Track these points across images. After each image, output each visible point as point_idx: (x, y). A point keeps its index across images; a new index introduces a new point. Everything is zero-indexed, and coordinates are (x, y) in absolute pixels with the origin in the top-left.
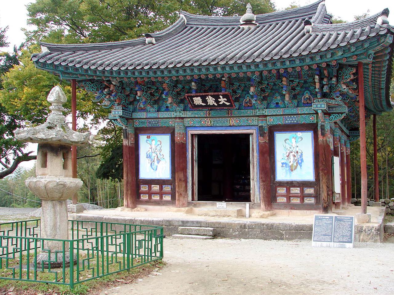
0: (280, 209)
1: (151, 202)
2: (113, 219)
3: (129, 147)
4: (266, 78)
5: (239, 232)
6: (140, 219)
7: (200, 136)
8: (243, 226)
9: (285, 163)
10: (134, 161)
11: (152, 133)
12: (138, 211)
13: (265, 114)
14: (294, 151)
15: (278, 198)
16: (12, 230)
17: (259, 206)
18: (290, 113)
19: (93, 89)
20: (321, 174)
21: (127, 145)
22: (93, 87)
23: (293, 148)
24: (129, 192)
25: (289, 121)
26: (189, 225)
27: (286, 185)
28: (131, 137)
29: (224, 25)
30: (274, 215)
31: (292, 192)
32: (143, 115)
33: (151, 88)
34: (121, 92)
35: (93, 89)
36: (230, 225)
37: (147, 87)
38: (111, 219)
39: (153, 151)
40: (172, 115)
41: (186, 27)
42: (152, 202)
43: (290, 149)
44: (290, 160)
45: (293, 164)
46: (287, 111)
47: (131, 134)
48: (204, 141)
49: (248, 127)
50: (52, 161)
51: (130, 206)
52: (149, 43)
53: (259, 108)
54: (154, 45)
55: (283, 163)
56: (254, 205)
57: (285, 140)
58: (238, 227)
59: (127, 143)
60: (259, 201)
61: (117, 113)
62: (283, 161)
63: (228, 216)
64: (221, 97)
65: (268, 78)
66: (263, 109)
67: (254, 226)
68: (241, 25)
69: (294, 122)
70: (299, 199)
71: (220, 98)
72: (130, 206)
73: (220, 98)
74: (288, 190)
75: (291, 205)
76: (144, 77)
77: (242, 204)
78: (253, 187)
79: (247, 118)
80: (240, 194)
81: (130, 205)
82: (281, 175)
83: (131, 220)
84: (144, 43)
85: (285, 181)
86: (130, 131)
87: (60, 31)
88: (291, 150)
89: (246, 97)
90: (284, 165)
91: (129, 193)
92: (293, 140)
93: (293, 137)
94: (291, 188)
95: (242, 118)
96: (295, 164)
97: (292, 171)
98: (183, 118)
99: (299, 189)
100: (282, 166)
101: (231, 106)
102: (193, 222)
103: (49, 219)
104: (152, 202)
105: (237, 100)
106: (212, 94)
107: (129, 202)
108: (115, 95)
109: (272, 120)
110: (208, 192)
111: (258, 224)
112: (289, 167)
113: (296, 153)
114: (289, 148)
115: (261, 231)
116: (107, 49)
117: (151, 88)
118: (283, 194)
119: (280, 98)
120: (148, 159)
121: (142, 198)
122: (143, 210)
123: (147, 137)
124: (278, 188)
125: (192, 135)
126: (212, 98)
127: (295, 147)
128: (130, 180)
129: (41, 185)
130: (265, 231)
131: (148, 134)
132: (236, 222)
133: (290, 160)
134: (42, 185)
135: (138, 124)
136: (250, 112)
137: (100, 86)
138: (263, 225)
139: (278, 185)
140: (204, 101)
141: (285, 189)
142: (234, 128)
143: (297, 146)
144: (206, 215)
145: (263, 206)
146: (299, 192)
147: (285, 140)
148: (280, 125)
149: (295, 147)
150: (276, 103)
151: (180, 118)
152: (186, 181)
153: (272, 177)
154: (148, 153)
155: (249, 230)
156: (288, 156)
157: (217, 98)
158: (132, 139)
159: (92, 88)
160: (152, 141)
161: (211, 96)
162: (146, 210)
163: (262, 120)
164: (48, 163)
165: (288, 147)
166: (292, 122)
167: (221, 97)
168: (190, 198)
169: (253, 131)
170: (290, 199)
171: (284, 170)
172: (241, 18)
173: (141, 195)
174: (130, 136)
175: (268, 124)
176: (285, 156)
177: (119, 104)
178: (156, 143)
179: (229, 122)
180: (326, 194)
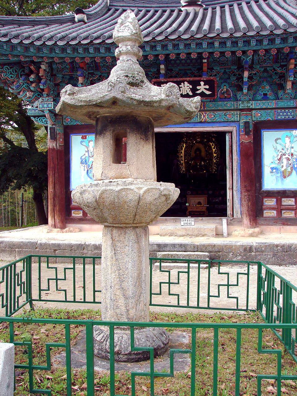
0: (268, 225)
1: (86, 220)
2: (53, 244)
3: (58, 151)
4: (259, 61)
5: (243, 257)
6: (93, 243)
8: (248, 249)
9: (276, 168)
10: (64, 167)
12: (71, 232)
13: (251, 107)
14: (287, 153)
15: (265, 211)
16: (57, 289)
17: (240, 221)
18: (286, 106)
19: (13, 76)
21: (54, 148)
22: (12, 72)
23: (286, 149)
24: (57, 208)
25: (282, 116)
26: (168, 249)
27: (276, 195)
28: (60, 138)
29: (159, 7)
30: (262, 233)
31: (283, 203)
33: (95, 74)
34: (50, 80)
35: (13, 76)
36: (229, 248)
37: (89, 73)
38: (49, 245)
39: (90, 155)
41: (109, 10)
42: (89, 220)
43: (283, 151)
44: (282, 164)
45: (286, 169)
46: (281, 104)
47: (60, 133)
49: (225, 124)
50: (139, 150)
51: (59, 226)
52: (79, 21)
53: (242, 99)
54: (86, 23)
55: (272, 169)
56: (233, 220)
57: (276, 140)
58: (241, 250)
59: (55, 146)
60: (239, 216)
61: (45, 106)
62: (273, 166)
63: (203, 236)
64: (202, 83)
65: (262, 62)
66: (248, 101)
67: (263, 249)
68: (183, 7)
69: (289, 117)
70: (293, 212)
71: (200, 85)
72: (59, 226)
73: (200, 85)
74: (279, 202)
75: (283, 219)
76: (85, 57)
77: (216, 219)
78: (231, 198)
79: (225, 112)
80: (217, 208)
81: (58, 225)
82: (270, 182)
83: (79, 245)
84: (72, 20)
85: (275, 190)
86: (59, 130)
88: (284, 152)
89: (222, 86)
90: (274, 171)
91: (57, 209)
92: (287, 140)
93: (287, 137)
94: (283, 199)
95: (219, 112)
96: (289, 169)
97: (285, 177)
99: (293, 199)
100: (272, 172)
102: (174, 245)
103: (130, 266)
104: (88, 220)
106: (191, 79)
107: (57, 221)
108: (45, 84)
109: (259, 115)
111: (269, 245)
112: (281, 173)
113: (290, 155)
114: (281, 150)
115: (274, 255)
116: (28, 24)
117: (95, 74)
118: (272, 207)
119: (269, 88)
120: (84, 165)
121: (73, 215)
122: (77, 230)
123: (82, 138)
124: (265, 199)
126: (188, 85)
127: (289, 148)
128: (58, 192)
129: (131, 197)
130: (279, 254)
131: (82, 133)
132: (239, 244)
133: (282, 164)
134: (131, 197)
136: (230, 104)
137: (21, 72)
138: (277, 246)
139: (265, 195)
141: (275, 200)
142: (206, 125)
143: (292, 148)
144: (171, 235)
145: (246, 221)
146: (293, 203)
147: (276, 140)
148: (269, 121)
149: (289, 148)
150: (264, 94)
153: (257, 185)
154: (83, 158)
155: (257, 253)
156: (279, 160)
158: (61, 140)
159: (11, 74)
160: (89, 142)
161: (189, 82)
162: (81, 230)
163: (247, 115)
164: (130, 153)
165: (279, 148)
166: (287, 117)
167: (202, 83)
169: (233, 128)
170: (281, 212)
171: (274, 177)
173: (73, 212)
174: (58, 137)
175: (254, 119)
176: (276, 159)
177: (48, 95)
179: (200, 117)
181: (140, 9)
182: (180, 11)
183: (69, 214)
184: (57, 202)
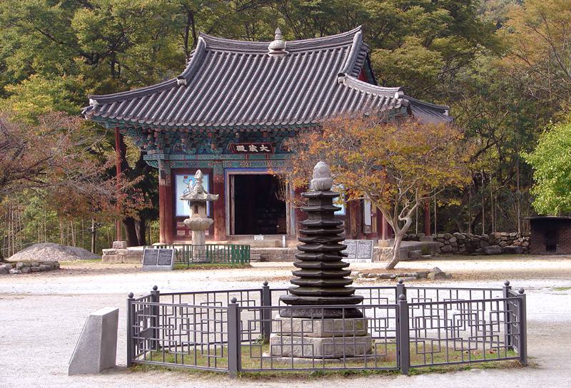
3: (166, 187)
7: (236, 176)
11: (190, 174)
20: (351, 209)
24: (167, 229)
32: (181, 157)
40: (212, 156)
48: (239, 179)
60: (294, 233)
86: (168, 172)
87: (176, 133)
98: (221, 160)
101: (271, 152)
105: (274, 145)
107: (167, 238)
110: (244, 227)
125: (230, 175)
135: (174, 166)
140: (247, 147)
151: (218, 160)
152: (224, 217)
157: (258, 147)
164: (199, 211)
168: (228, 233)
172: (270, 45)
178: (194, 183)
180: (355, 226)
181: (234, 52)
182: (268, 56)
183: (175, 233)
184: (166, 224)
